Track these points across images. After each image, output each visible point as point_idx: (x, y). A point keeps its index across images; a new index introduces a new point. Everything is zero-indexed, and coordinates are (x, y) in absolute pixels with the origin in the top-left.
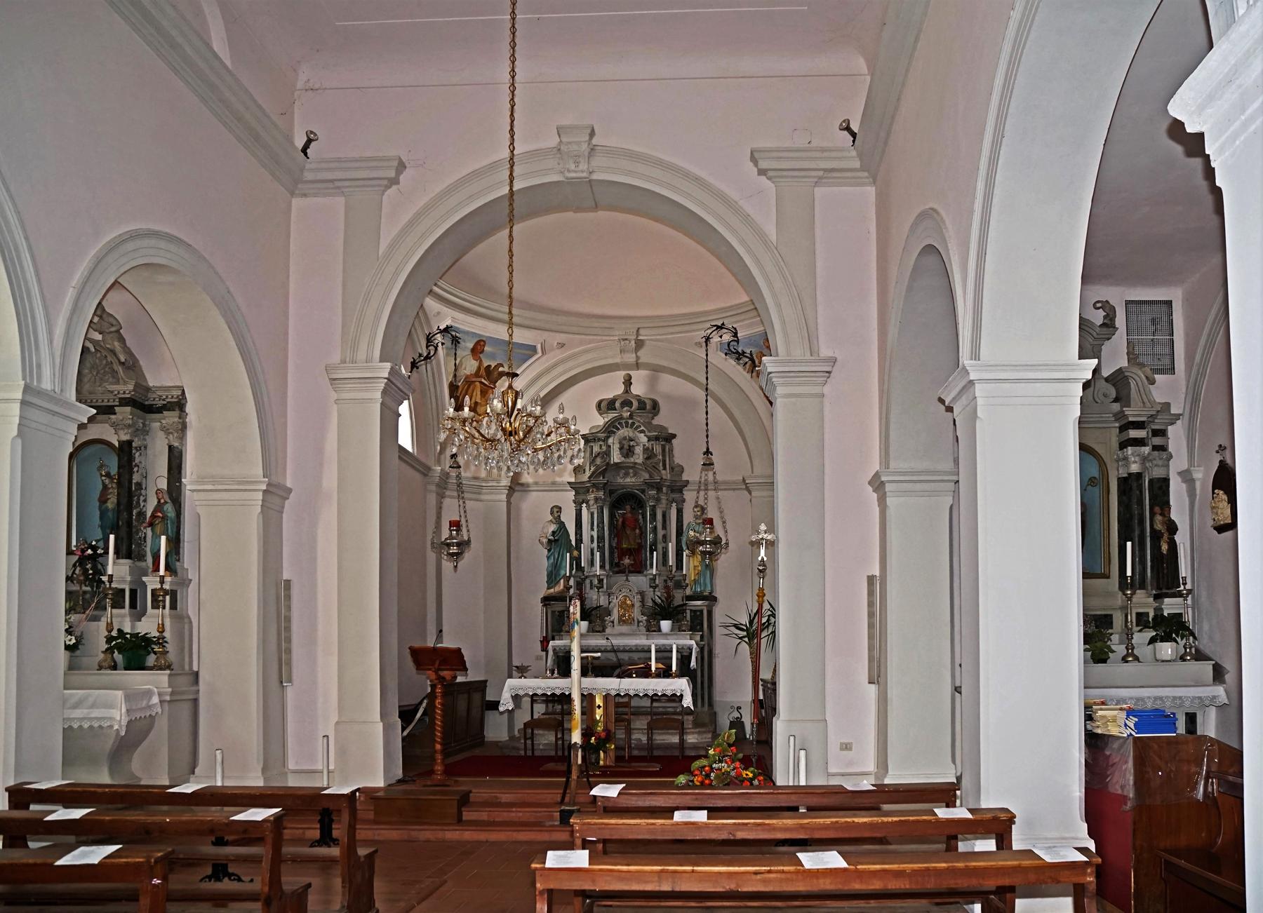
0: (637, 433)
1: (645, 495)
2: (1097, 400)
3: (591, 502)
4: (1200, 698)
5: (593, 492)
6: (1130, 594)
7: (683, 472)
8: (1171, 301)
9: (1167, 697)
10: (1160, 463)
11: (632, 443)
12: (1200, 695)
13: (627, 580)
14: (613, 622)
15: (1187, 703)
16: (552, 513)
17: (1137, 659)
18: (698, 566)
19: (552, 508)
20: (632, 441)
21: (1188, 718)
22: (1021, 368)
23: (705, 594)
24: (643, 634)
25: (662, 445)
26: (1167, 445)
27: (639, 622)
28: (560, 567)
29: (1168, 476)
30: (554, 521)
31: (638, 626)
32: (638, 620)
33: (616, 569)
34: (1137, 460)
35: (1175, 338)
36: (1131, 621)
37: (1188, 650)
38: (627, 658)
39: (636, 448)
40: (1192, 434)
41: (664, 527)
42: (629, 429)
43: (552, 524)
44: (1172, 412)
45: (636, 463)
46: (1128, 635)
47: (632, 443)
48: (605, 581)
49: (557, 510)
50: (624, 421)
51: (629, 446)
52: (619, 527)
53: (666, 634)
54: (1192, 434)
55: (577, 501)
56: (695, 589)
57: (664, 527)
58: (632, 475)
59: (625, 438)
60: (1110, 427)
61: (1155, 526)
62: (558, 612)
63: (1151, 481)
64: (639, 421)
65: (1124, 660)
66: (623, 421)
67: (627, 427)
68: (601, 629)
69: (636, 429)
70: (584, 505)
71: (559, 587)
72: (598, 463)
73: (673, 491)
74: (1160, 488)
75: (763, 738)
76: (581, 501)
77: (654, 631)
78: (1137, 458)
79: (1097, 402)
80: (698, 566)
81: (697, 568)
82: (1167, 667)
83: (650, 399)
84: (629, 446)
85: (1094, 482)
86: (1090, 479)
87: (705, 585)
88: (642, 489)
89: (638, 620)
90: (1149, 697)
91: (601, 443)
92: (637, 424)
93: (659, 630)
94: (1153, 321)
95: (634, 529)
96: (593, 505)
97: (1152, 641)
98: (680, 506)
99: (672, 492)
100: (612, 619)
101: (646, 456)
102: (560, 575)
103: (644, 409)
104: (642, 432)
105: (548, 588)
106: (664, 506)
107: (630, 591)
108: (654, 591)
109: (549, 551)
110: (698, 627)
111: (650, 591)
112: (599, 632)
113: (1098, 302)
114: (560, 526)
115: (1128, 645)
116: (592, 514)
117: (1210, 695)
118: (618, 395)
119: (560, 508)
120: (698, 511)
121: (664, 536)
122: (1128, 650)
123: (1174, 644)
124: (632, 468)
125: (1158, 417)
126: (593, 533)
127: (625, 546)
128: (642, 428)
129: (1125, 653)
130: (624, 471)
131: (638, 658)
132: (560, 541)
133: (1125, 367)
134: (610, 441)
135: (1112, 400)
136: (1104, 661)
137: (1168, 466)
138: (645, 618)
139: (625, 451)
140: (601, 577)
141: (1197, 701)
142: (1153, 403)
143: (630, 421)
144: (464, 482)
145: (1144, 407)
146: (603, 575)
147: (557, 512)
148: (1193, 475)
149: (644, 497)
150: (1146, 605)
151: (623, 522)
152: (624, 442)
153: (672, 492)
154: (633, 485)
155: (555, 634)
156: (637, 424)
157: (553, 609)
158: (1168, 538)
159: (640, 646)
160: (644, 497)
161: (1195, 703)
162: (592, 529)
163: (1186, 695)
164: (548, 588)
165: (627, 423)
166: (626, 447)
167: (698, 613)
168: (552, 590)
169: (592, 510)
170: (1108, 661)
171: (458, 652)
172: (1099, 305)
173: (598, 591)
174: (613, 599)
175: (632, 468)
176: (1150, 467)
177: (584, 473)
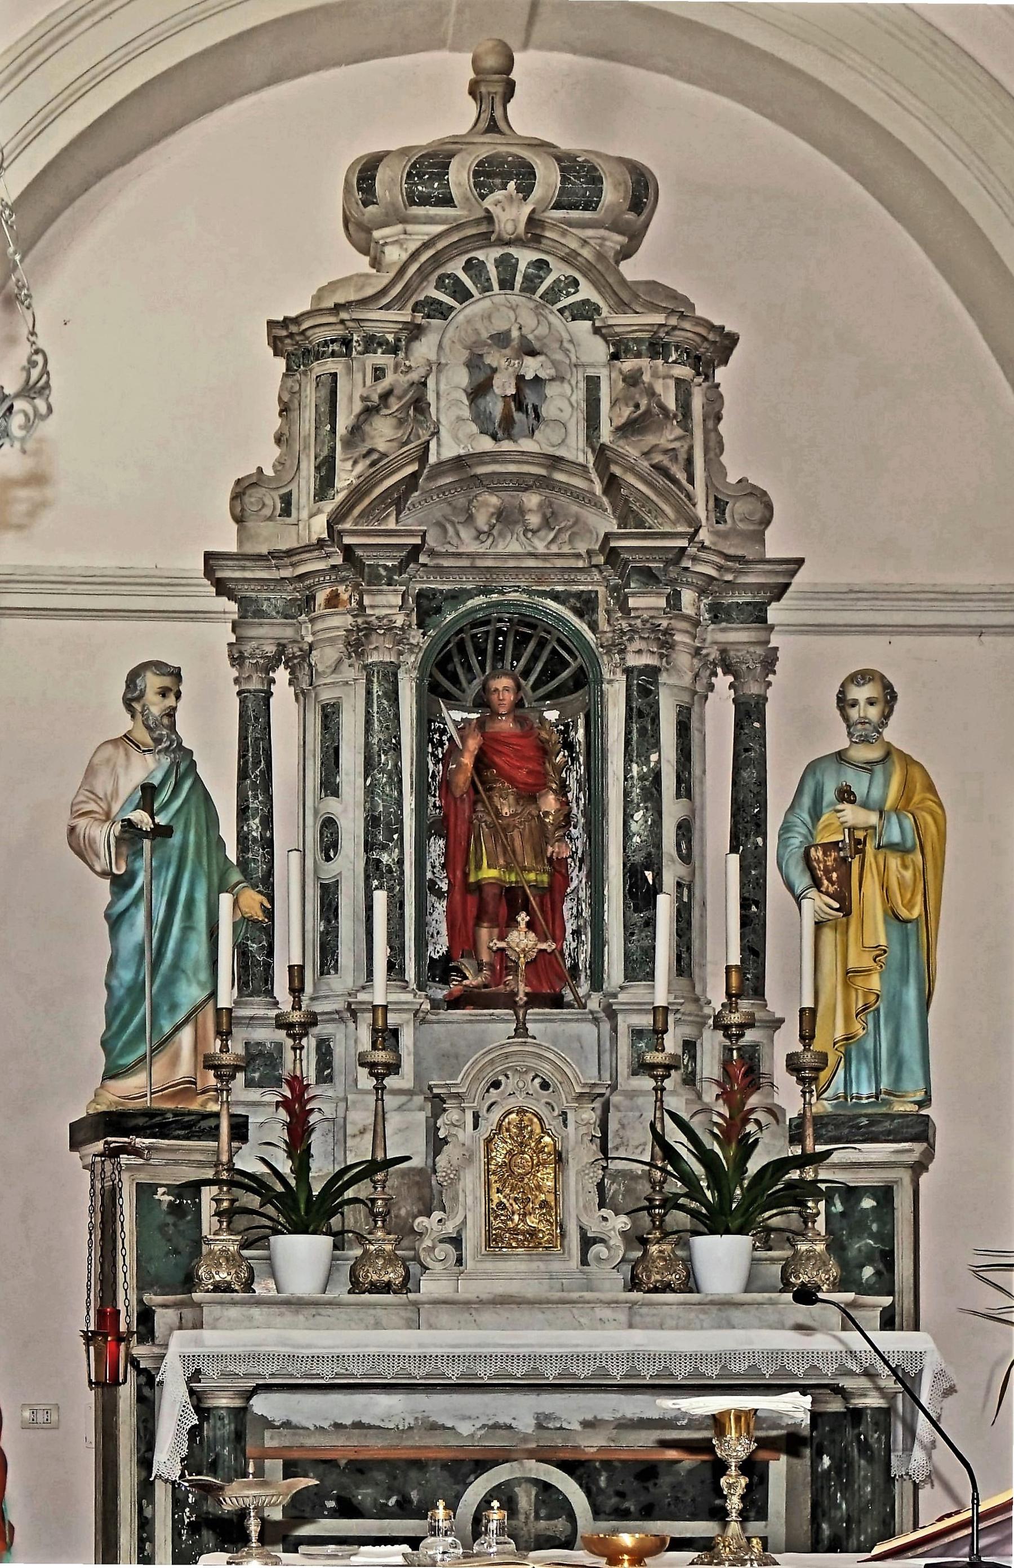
0: (555, 320)
1: (593, 627)
3: (324, 657)
5: (333, 601)
7: (767, 521)
11: (531, 367)
13: (521, 1031)
14: (456, 1241)
16: (132, 699)
18: (867, 972)
19: (133, 677)
20: (533, 353)
22: (824, 596)
23: (899, 1108)
24: (613, 1303)
25: (679, 382)
27: (587, 1242)
28: (176, 966)
30: (143, 736)
31: (584, 1262)
32: (583, 1231)
33: (440, 993)
38: (526, 1425)
39: (551, 390)
41: (685, 788)
42: (515, 297)
43: (135, 755)
45: (555, 462)
47: (531, 367)
48: (407, 1039)
49: (167, 681)
50: (496, 252)
51: (520, 379)
52: (462, 781)
53: (726, 1304)
55: (248, 648)
56: (847, 1082)
57: (685, 788)
58: (534, 520)
59: (501, 339)
62: (171, 1189)
64: (570, 258)
66: (488, 256)
67: (506, 284)
68: (393, 1275)
69: (552, 295)
70: (281, 675)
71: (174, 1061)
72: (382, 446)
73: (718, 613)
76: (270, 649)
77: (666, 1288)
80: (867, 972)
81: (859, 981)
83: (621, 160)
84: (520, 379)
87: (898, 1063)
88: (579, 595)
89: (583, 1231)
91: (380, 358)
92: (558, 271)
93: (690, 1284)
95: (529, 796)
96: (336, 668)
98: (753, 689)
99: (715, 619)
100: (450, 1228)
101: (626, 412)
102: (174, 1007)
103: (589, 205)
104: (584, 311)
105: (112, 1073)
106: (687, 680)
107: (545, 1086)
108: (660, 1090)
109: (121, 883)
110: (868, 1272)
111: (632, 1095)
112: (387, 1288)
114: (175, 764)
116: (330, 716)
118: (455, 140)
119: (176, 675)
120: (871, 702)
121: (685, 829)
124: (524, 483)
126: (332, 806)
127: (488, 873)
128: (586, 292)
130: (494, 500)
131: (586, 1424)
132: (176, 839)
134: (424, 349)
138: (622, 1222)
139: (496, 408)
140: (393, 1019)
143: (525, 257)
144: (548, 234)
146: (400, 1008)
147: (164, 693)
149: (589, 635)
151: (481, 762)
152: (493, 358)
153: (715, 619)
154: (540, 575)
155: (152, 1298)
156: (558, 271)
157: (143, 1178)
159: (651, 1358)
160: (589, 635)
162: (330, 787)
164: (112, 1073)
165: (508, 265)
166: (504, 385)
167: (868, 1203)
168: (134, 1083)
169: (326, 695)
171: (788, 1055)
173: (380, 1089)
174: (460, 1125)
175: (524, 483)
177: (286, 512)
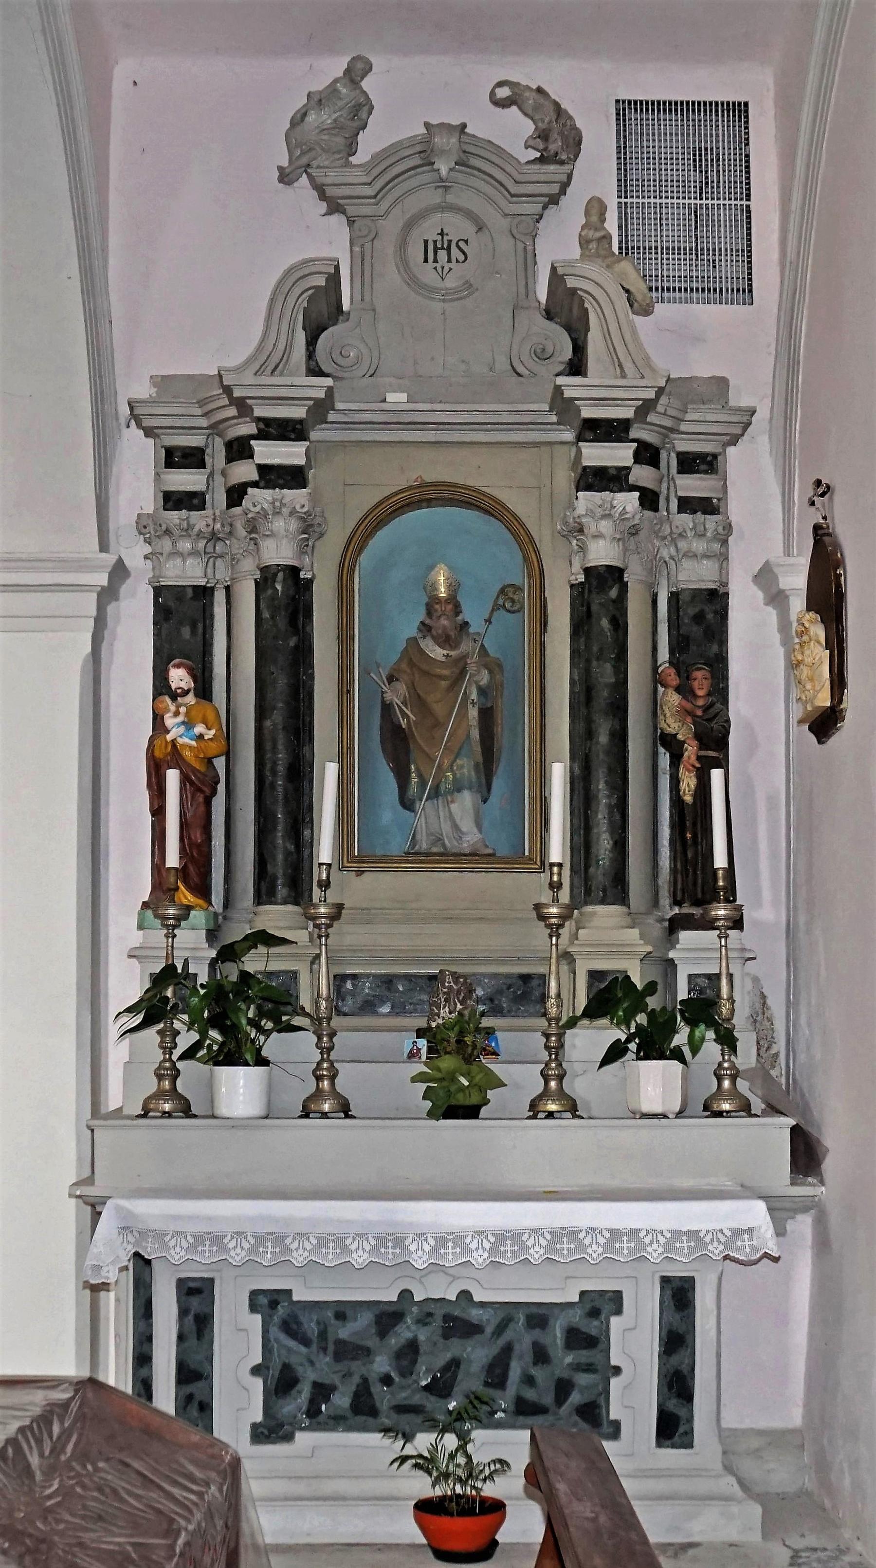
2: (521, 369)
4: (693, 1235)
6: (559, 917)
8: (746, 104)
9: (592, 1231)
10: (700, 546)
12: (693, 1227)
15: (655, 1253)
17: (572, 1108)
21: (669, 1292)
26: (723, 499)
29: (726, 585)
34: (604, 530)
35: (754, 204)
36: (558, 995)
37: (553, 1084)
40: (790, 465)
44: (732, 403)
46: (547, 1036)
54: (790, 465)
60: (550, 444)
61: (662, 725)
63: (674, 598)
65: (534, 1109)
74: (699, 618)
75: (195, 1302)
78: (604, 523)
79: (520, 375)
82: (647, 1131)
85: (513, 601)
86: (502, 591)
90: (536, 1231)
94: (698, 158)
97: (615, 1053)
113: (500, 84)
115: (547, 1064)
117: (727, 1225)
122: (546, 1079)
123: (675, 1066)
125: (688, 417)
129: (540, 1089)
133: (570, 263)
135: (561, 368)
136: (472, 1112)
137: (723, 558)
141: (684, 1244)
142: (645, 366)
145: (623, 376)
148: (781, 579)
150: (621, 950)
158: (699, 758)
161: (680, 1251)
163: (710, 1227)
170: (484, 1112)
172: (504, 93)
176: (672, 558)
